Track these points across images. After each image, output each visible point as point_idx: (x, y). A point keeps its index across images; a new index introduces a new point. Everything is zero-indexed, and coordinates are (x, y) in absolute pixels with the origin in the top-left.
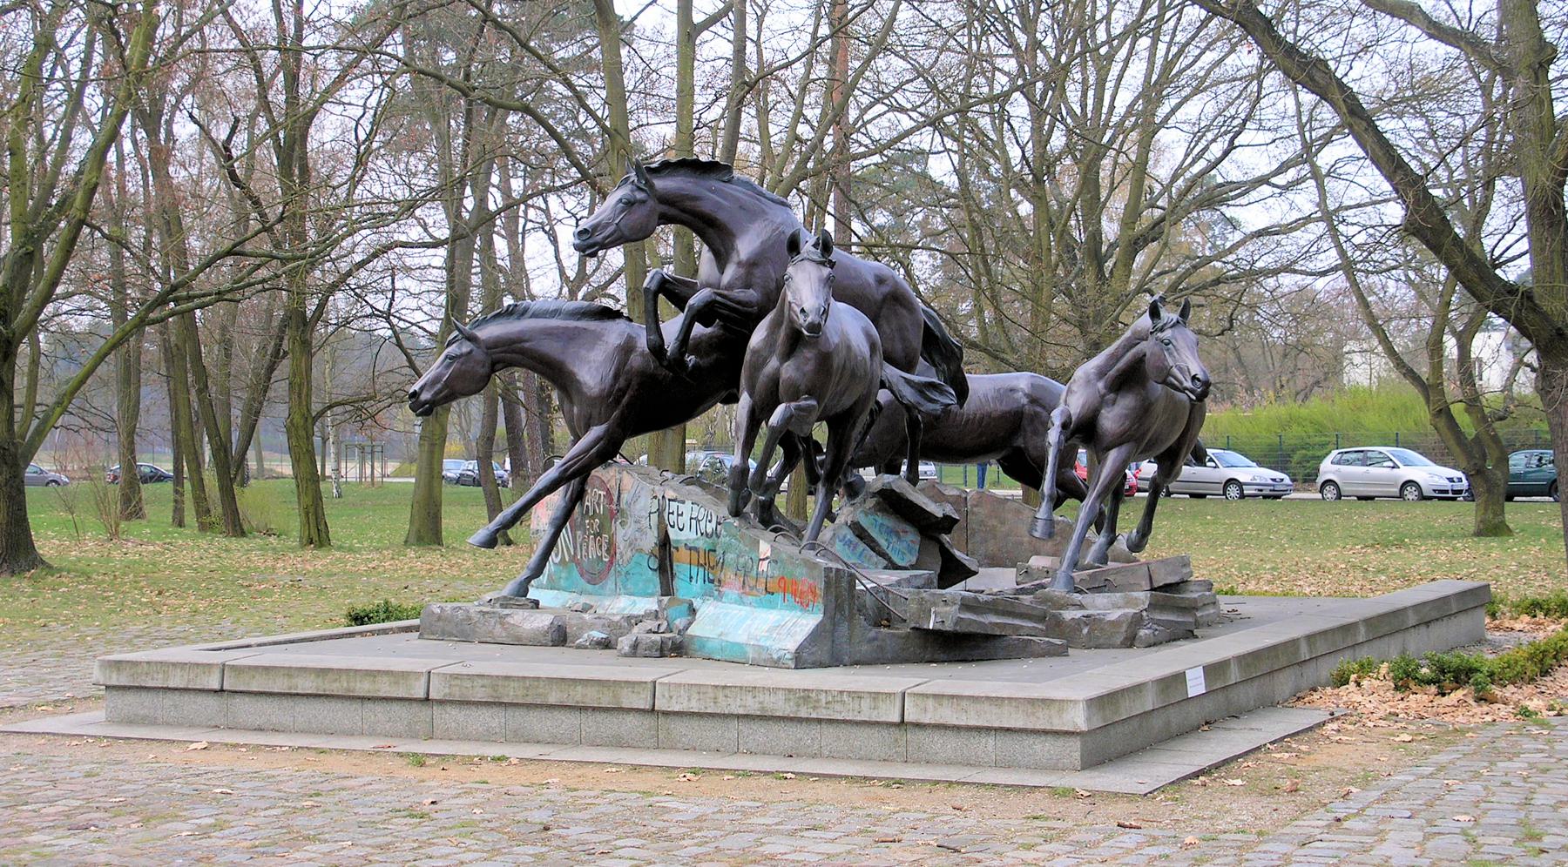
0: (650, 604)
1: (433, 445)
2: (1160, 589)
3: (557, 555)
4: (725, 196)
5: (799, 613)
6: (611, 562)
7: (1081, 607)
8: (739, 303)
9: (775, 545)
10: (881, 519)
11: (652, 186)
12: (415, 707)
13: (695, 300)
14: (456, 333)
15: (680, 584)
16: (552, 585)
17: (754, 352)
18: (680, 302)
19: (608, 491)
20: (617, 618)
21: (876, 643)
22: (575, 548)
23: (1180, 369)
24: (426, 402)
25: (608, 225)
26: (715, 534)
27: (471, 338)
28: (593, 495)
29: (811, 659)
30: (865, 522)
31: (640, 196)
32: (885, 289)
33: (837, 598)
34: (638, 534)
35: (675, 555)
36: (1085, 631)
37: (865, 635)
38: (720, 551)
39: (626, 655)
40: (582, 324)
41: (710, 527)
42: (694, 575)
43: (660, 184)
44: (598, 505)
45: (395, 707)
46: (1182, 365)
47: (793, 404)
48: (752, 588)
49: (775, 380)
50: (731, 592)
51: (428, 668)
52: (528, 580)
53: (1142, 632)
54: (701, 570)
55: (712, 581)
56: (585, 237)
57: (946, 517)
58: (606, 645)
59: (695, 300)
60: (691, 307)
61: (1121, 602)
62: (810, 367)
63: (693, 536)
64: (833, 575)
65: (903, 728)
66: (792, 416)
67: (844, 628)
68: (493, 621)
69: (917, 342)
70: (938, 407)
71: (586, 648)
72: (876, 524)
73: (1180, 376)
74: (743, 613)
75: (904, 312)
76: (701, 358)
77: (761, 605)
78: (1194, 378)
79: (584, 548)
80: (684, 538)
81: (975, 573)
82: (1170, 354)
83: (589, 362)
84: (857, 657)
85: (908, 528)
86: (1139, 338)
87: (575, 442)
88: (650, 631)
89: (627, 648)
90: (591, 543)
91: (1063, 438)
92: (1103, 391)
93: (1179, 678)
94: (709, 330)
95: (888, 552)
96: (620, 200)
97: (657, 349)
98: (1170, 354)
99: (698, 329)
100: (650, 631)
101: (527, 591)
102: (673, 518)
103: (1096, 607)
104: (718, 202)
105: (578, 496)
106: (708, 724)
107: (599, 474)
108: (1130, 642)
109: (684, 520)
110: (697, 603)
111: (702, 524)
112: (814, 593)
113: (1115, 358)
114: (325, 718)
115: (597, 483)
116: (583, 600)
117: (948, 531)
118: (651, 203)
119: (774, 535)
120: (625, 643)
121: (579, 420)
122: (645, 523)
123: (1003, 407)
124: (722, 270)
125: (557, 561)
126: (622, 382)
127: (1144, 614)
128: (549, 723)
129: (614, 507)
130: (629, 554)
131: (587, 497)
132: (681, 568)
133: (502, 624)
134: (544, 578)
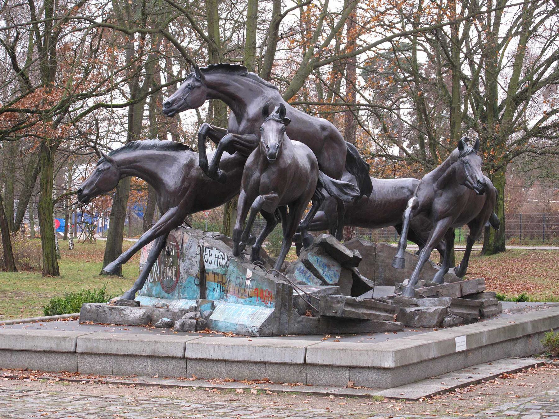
0: (193, 304)
1: (118, 219)
3: (152, 278)
4: (242, 84)
5: (263, 308)
6: (177, 281)
7: (417, 305)
8: (244, 141)
9: (255, 271)
11: (204, 78)
12: (70, 356)
13: (225, 139)
16: (149, 295)
17: (248, 168)
18: (216, 140)
19: (177, 243)
20: (177, 311)
21: (301, 324)
22: (160, 274)
23: (472, 177)
24: (86, 195)
25: (180, 100)
26: (227, 266)
28: (171, 244)
31: (197, 84)
32: (326, 133)
33: (282, 299)
36: (416, 318)
38: (228, 275)
39: (178, 331)
42: (216, 287)
43: (208, 77)
47: (264, 196)
49: (258, 182)
50: (231, 297)
51: (76, 336)
52: (135, 291)
53: (447, 319)
54: (219, 285)
55: (223, 291)
56: (168, 106)
57: (355, 257)
58: (170, 325)
60: (221, 143)
61: (437, 303)
62: (274, 176)
63: (216, 267)
64: (280, 287)
66: (264, 202)
67: (285, 316)
69: (342, 160)
70: (350, 197)
73: (472, 181)
74: (237, 307)
75: (336, 145)
76: (227, 171)
77: (246, 303)
78: (478, 182)
80: (211, 268)
81: (371, 288)
82: (468, 169)
83: (170, 173)
84: (292, 331)
85: (335, 263)
86: (454, 159)
87: (162, 216)
89: (179, 326)
91: (412, 214)
92: (436, 189)
93: (452, 342)
94: (233, 156)
95: (323, 276)
97: (204, 164)
98: (468, 169)
99: (226, 155)
100: (191, 318)
101: (134, 297)
102: (207, 257)
104: (238, 87)
105: (162, 246)
106: (210, 364)
109: (212, 258)
110: (216, 303)
111: (221, 260)
113: (442, 170)
114: (26, 362)
115: (172, 238)
116: (164, 301)
117: (357, 265)
118: (203, 88)
119: (255, 265)
120: (178, 324)
121: (163, 204)
122: (193, 259)
124: (239, 122)
125: (151, 281)
126: (186, 184)
127: (448, 309)
128: (134, 365)
129: (180, 252)
130: (186, 276)
131: (167, 246)
132: (210, 284)
134: (144, 290)
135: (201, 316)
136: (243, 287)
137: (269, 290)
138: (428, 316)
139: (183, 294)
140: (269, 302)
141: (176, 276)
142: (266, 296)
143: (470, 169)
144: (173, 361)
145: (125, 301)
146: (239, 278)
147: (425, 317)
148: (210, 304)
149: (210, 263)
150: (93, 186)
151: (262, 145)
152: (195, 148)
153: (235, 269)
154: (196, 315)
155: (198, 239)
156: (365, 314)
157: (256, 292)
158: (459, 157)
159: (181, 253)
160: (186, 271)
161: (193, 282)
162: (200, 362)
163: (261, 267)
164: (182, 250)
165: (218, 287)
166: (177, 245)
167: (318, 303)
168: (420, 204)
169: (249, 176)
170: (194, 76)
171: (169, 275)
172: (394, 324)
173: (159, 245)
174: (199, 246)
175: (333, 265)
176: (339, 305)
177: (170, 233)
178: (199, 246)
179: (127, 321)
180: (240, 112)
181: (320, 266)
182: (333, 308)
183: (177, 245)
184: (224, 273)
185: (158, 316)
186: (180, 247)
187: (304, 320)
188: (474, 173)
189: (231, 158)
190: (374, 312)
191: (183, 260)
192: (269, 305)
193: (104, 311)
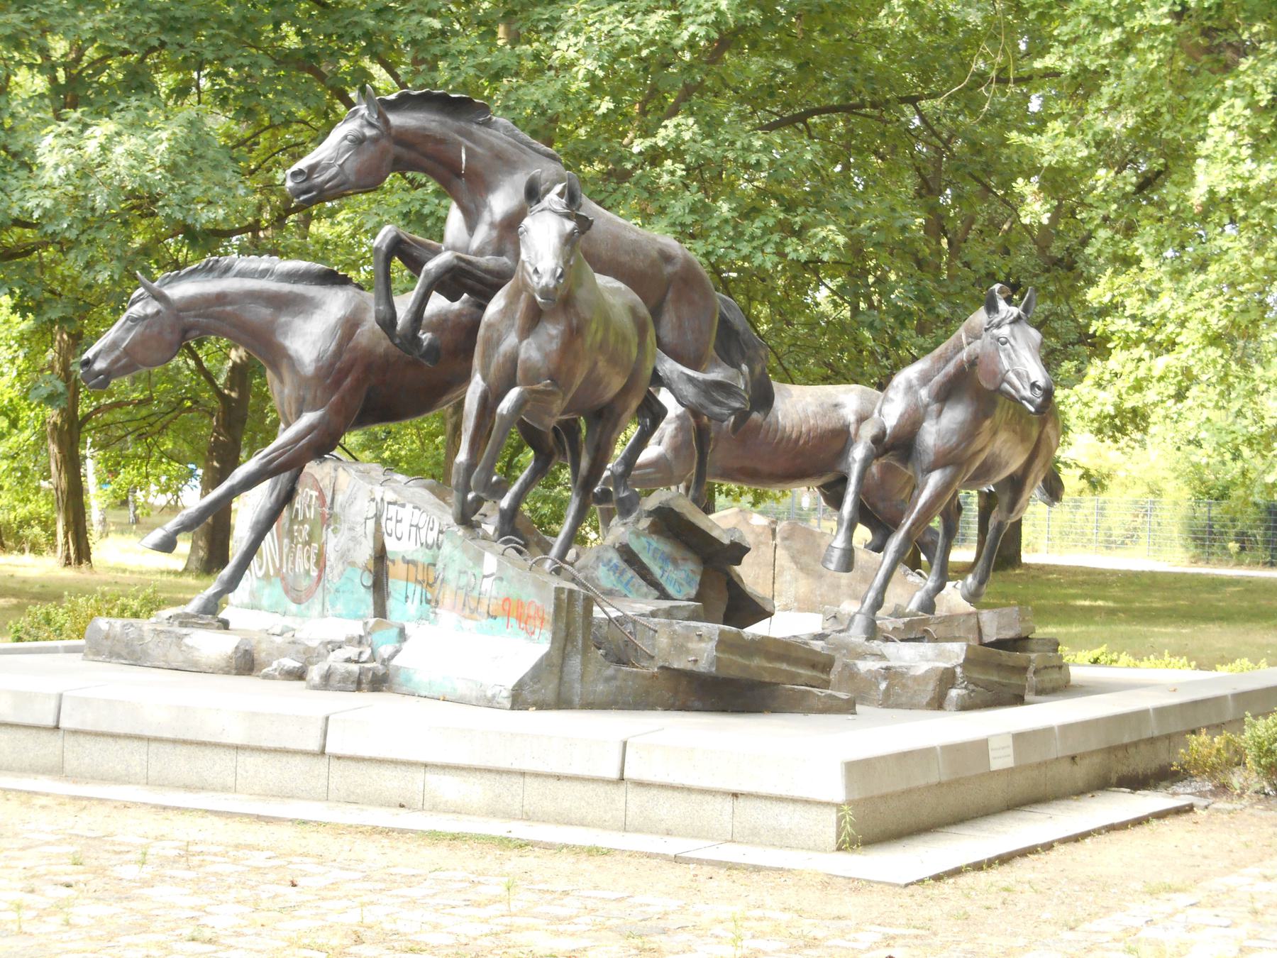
0: (357, 629)
2: (992, 645)
3: (260, 568)
7: (882, 657)
10: (657, 543)
11: (387, 122)
12: (44, 736)
13: (432, 265)
14: (141, 290)
15: (392, 604)
17: (490, 326)
18: (415, 265)
19: (321, 491)
21: (615, 683)
22: (281, 559)
23: (1018, 375)
24: (100, 373)
25: (329, 166)
27: (160, 297)
28: (305, 495)
29: (530, 698)
30: (636, 546)
31: (369, 132)
33: (568, 625)
34: (351, 544)
35: (392, 569)
37: (603, 675)
38: (440, 565)
39: (315, 688)
40: (299, 288)
41: (432, 537)
42: (410, 594)
43: (395, 119)
44: (309, 507)
45: (21, 734)
46: (1020, 369)
48: (473, 611)
49: (513, 359)
55: (428, 602)
56: (300, 179)
58: (299, 675)
59: (432, 265)
60: (428, 273)
62: (554, 346)
64: (564, 596)
65: (622, 788)
68: (169, 640)
71: (273, 678)
72: (650, 549)
78: (1033, 385)
79: (291, 559)
82: (1009, 356)
85: (689, 555)
88: (348, 660)
90: (299, 554)
94: (457, 305)
95: (662, 581)
96: (345, 138)
98: (1009, 356)
99: (438, 303)
100: (348, 660)
103: (899, 659)
105: (287, 497)
107: (311, 471)
108: (938, 703)
109: (403, 528)
111: (423, 532)
112: (543, 620)
115: (310, 481)
118: (384, 142)
119: (504, 547)
120: (315, 674)
122: (360, 530)
123: (824, 424)
125: (260, 574)
129: (327, 511)
132: (396, 586)
133: (179, 646)
135: (373, 658)
136: (475, 593)
137: (538, 603)
138: (910, 683)
139: (333, 606)
140: (537, 631)
141: (317, 564)
142: (529, 617)
143: (1013, 356)
144: (298, 760)
145: (193, 616)
146: (465, 572)
147: (904, 686)
148: (395, 632)
149: (399, 539)
150: (117, 353)
151: (523, 267)
152: (367, 281)
153: (457, 554)
154: (361, 653)
155: (371, 483)
156: (765, 669)
157: (507, 607)
158: (986, 330)
159: (331, 515)
160: (342, 556)
161: (357, 581)
162: (362, 766)
163: (520, 552)
164: (331, 508)
165: (416, 590)
166: (321, 497)
167: (653, 637)
168: (888, 431)
169: (492, 344)
170: (363, 116)
171: (303, 563)
172: (830, 696)
173: (278, 495)
174: (373, 500)
175: (684, 559)
176: (703, 645)
177: (306, 469)
178: (373, 500)
179: (196, 664)
180: (473, 206)
181: (654, 558)
182: (688, 652)
183: (321, 497)
184: (430, 561)
185: (269, 654)
186: (328, 500)
187: (620, 675)
188: (1023, 365)
189: (452, 312)
190: (784, 666)
191: (335, 531)
192: (535, 637)
193: (141, 638)
